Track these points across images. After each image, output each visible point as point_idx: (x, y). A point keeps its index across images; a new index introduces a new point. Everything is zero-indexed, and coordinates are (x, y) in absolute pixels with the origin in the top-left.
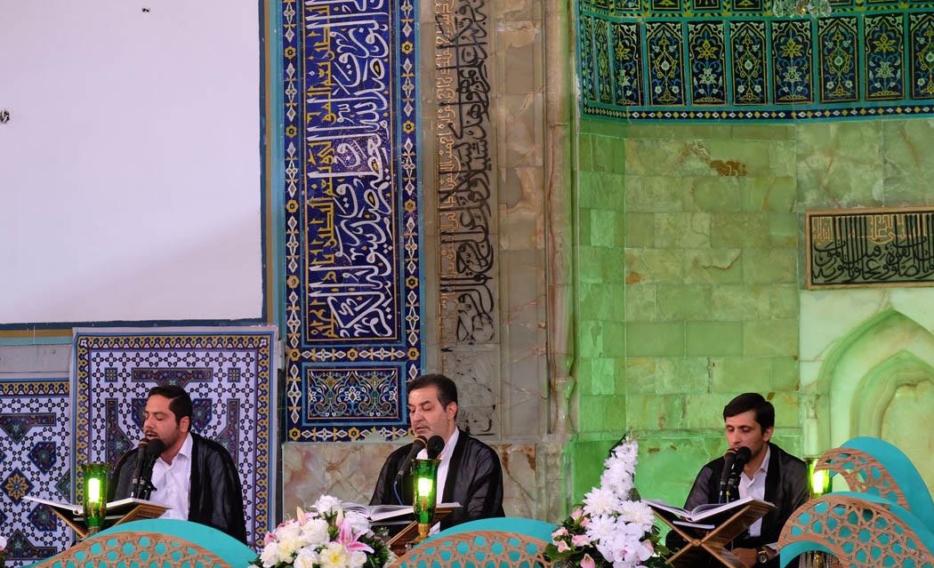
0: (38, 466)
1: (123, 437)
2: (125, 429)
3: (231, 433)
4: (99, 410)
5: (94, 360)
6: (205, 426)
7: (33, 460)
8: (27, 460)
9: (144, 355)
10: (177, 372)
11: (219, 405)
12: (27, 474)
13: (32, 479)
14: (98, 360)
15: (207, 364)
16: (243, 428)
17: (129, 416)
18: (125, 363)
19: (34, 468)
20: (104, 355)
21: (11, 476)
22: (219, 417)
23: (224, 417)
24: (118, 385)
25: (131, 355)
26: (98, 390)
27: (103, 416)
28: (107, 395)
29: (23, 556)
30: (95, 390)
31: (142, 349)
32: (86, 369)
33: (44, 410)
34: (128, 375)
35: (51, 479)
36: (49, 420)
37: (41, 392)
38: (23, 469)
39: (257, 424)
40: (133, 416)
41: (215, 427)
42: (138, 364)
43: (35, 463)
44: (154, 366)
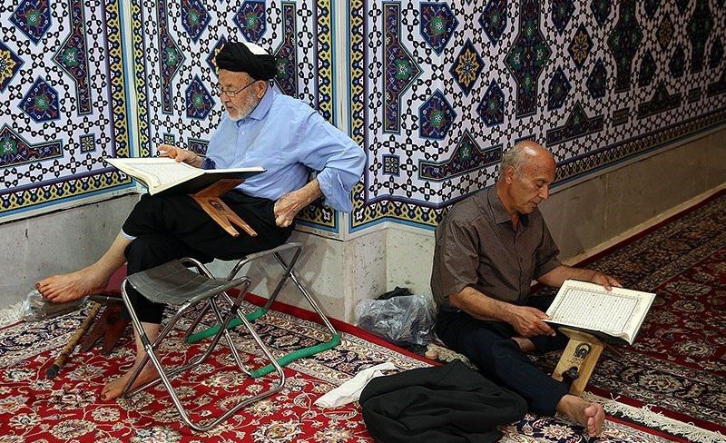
0: (26, 33)
2: (65, 78)
3: (77, 39)
4: (100, 98)
7: (240, 27)
9: (49, 176)
13: (20, 52)
17: (61, 96)
19: (21, 36)
24: (78, 133)
25: (66, 173)
26: (102, 122)
27: (94, 91)
28: (92, 118)
29: (17, 161)
30: (106, 121)
31: (51, 183)
32: (118, 145)
34: (67, 148)
35: (45, 50)
39: (106, 26)
40: (57, 97)
42: (56, 163)
43: (22, 29)
44: (35, 165)
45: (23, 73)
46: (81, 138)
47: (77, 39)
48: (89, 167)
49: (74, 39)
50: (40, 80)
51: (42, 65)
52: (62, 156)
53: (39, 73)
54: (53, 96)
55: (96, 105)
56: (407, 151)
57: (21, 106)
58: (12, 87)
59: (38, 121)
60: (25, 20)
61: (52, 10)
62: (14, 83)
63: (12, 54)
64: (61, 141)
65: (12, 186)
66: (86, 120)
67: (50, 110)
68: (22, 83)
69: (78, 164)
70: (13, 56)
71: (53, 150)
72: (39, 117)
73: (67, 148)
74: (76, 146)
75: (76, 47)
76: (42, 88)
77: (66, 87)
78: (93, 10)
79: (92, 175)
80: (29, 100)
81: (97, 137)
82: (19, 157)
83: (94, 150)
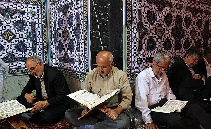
0: (17, 44)
1: (10, 16)
3: (2, 11)
4: (20, 7)
5: (38, 7)
6: (17, 49)
8: (20, 40)
10: (35, 38)
11: (25, 54)
12: (14, 40)
13: (12, 42)
14: (38, 9)
15: (22, 8)
16: (17, 64)
17: (19, 19)
18: (37, 19)
19: (17, 43)
20: (40, 11)
21: (13, 34)
22: (21, 55)
23: (21, 56)
25: (40, 21)
28: (26, 11)
32: (35, 4)
33: (38, 47)
34: (33, 20)
36: (22, 12)
37: (44, 46)
38: (16, 39)
41: (17, 53)
42: (37, 23)
43: (19, 43)
44: (37, 29)
45: (6, 42)
46: (35, 11)
47: (15, 59)
48: (40, 14)
49: (15, 58)
50: (13, 25)
51: (8, 48)
52: (35, 21)
53: (11, 24)
54: (19, 21)
55: (22, 8)
56: (6, 45)
57: (21, 31)
58: (2, 39)
59: (25, 27)
60: (21, 44)
61: (23, 52)
62: (14, 32)
63: (12, 40)
64: (31, 21)
65: (41, 36)
66: (26, 12)
67: (23, 23)
68: (3, 42)
69: (38, 17)
70: (11, 40)
71: (33, 24)
72: (25, 46)
73: (33, 20)
74: (33, 17)
75: (13, 59)
76: (16, 24)
77: (29, 44)
78: (24, 64)
79: (42, 13)
80: (19, 29)
81: (31, 10)
82: (34, 34)
83: (31, 15)
